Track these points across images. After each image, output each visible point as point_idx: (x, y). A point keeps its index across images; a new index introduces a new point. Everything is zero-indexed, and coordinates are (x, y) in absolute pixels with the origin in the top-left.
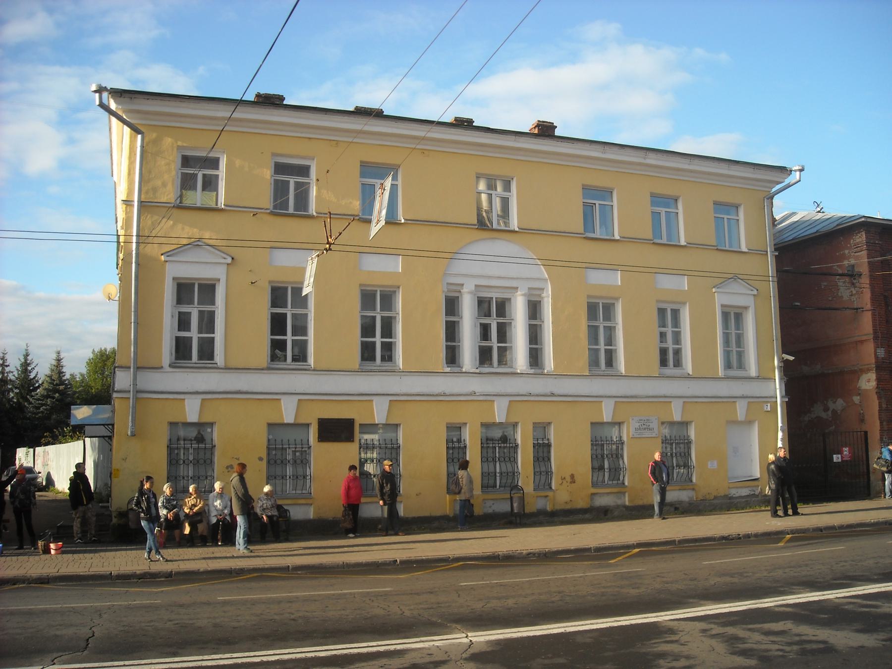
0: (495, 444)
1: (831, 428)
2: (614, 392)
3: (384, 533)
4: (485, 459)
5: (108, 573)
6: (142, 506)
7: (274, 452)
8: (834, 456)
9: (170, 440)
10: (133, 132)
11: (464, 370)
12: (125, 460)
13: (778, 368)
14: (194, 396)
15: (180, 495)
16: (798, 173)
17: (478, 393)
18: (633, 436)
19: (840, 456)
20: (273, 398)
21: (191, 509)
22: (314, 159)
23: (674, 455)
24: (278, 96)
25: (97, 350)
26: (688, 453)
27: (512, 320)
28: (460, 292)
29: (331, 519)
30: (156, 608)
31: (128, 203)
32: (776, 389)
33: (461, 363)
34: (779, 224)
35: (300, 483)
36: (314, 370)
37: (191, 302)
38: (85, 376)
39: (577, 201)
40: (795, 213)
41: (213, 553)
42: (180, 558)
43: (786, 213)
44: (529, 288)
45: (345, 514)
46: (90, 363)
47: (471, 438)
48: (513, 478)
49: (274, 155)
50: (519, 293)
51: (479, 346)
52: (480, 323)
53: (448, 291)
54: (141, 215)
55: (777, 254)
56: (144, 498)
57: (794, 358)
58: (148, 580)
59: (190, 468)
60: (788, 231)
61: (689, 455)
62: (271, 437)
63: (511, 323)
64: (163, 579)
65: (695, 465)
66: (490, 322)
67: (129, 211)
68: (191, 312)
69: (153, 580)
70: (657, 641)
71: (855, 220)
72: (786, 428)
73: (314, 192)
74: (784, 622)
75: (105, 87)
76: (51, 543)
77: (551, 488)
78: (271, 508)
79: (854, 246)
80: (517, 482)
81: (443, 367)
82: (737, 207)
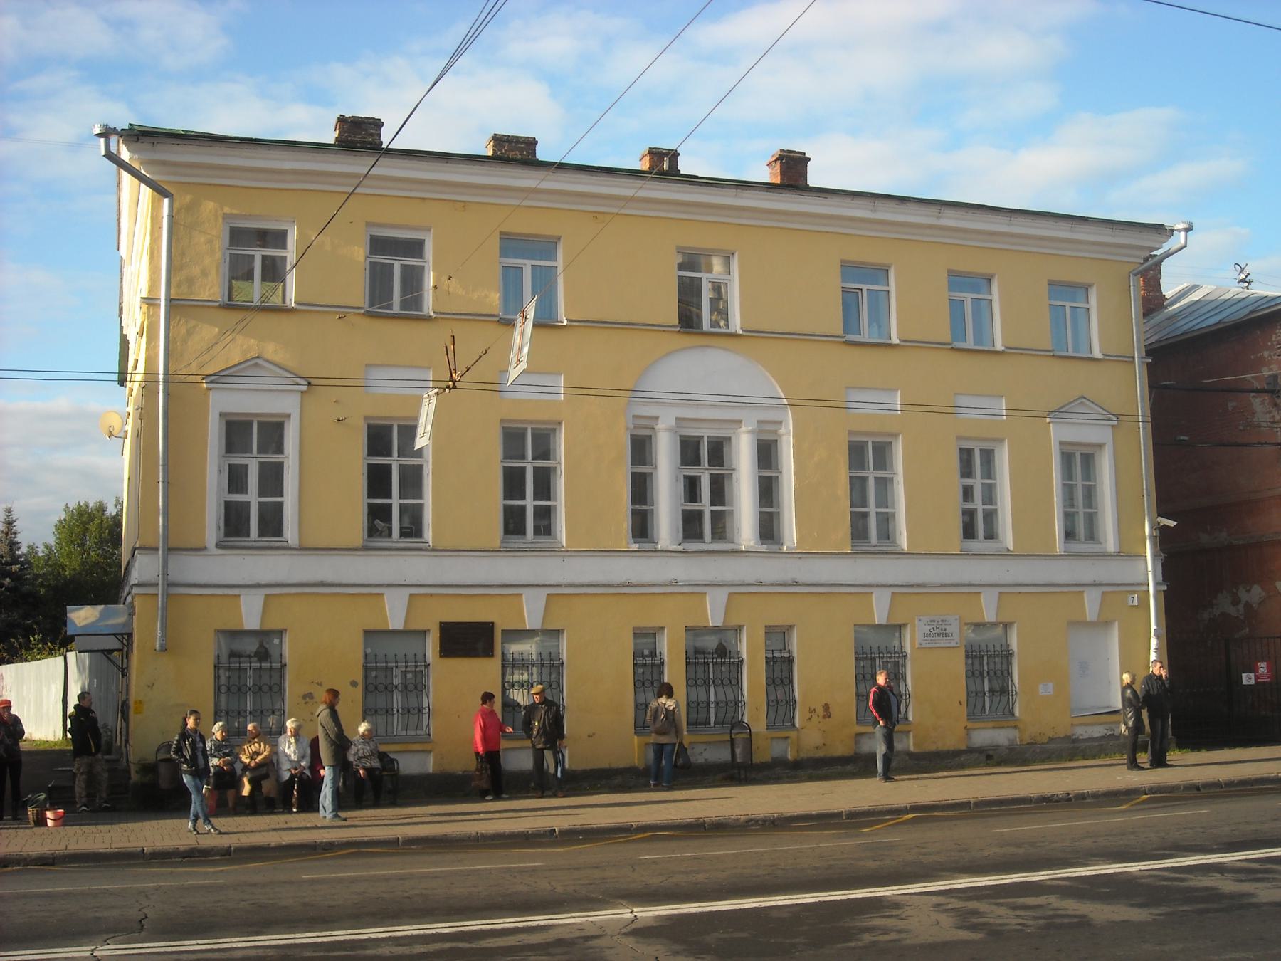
0: (708, 659)
1: (1244, 631)
2: (890, 580)
3: (540, 794)
4: (691, 683)
5: (139, 849)
6: (184, 753)
7: (374, 674)
8: (1244, 675)
9: (218, 656)
10: (156, 194)
11: (659, 547)
12: (151, 686)
13: (1150, 538)
14: (253, 591)
15: (234, 739)
16: (1183, 234)
17: (680, 581)
18: (920, 646)
19: (1252, 675)
20: (372, 593)
21: (252, 758)
22: (429, 230)
23: (985, 674)
24: (371, 120)
25: (72, 505)
26: (1008, 672)
27: (734, 470)
28: (653, 428)
29: (461, 773)
30: (221, 888)
31: (150, 301)
32: (1147, 571)
33: (655, 536)
34: (1171, 305)
35: (413, 719)
36: (433, 550)
37: (246, 449)
38: (53, 549)
39: (834, 284)
40: (1198, 286)
41: (286, 823)
42: (238, 830)
43: (1185, 285)
44: (758, 422)
45: (481, 767)
46: (60, 527)
47: (671, 650)
48: (736, 711)
49: (369, 224)
50: (743, 429)
51: (683, 510)
52: (684, 475)
53: (635, 427)
54: (171, 319)
55: (1150, 361)
56: (187, 743)
57: (1175, 523)
58: (197, 859)
59: (248, 700)
60: (1181, 317)
61: (1010, 674)
62: (369, 651)
63: (731, 474)
64: (218, 858)
65: (1017, 691)
66: (699, 474)
67: (152, 315)
68: (247, 465)
69: (203, 859)
70: (872, 915)
71: (1276, 305)
72: (1164, 631)
73: (430, 280)
74: (1046, 897)
75: (115, 128)
76: (47, 810)
77: (794, 725)
78: (370, 756)
79: (1277, 345)
80: (742, 715)
81: (628, 543)
82: (1086, 288)
